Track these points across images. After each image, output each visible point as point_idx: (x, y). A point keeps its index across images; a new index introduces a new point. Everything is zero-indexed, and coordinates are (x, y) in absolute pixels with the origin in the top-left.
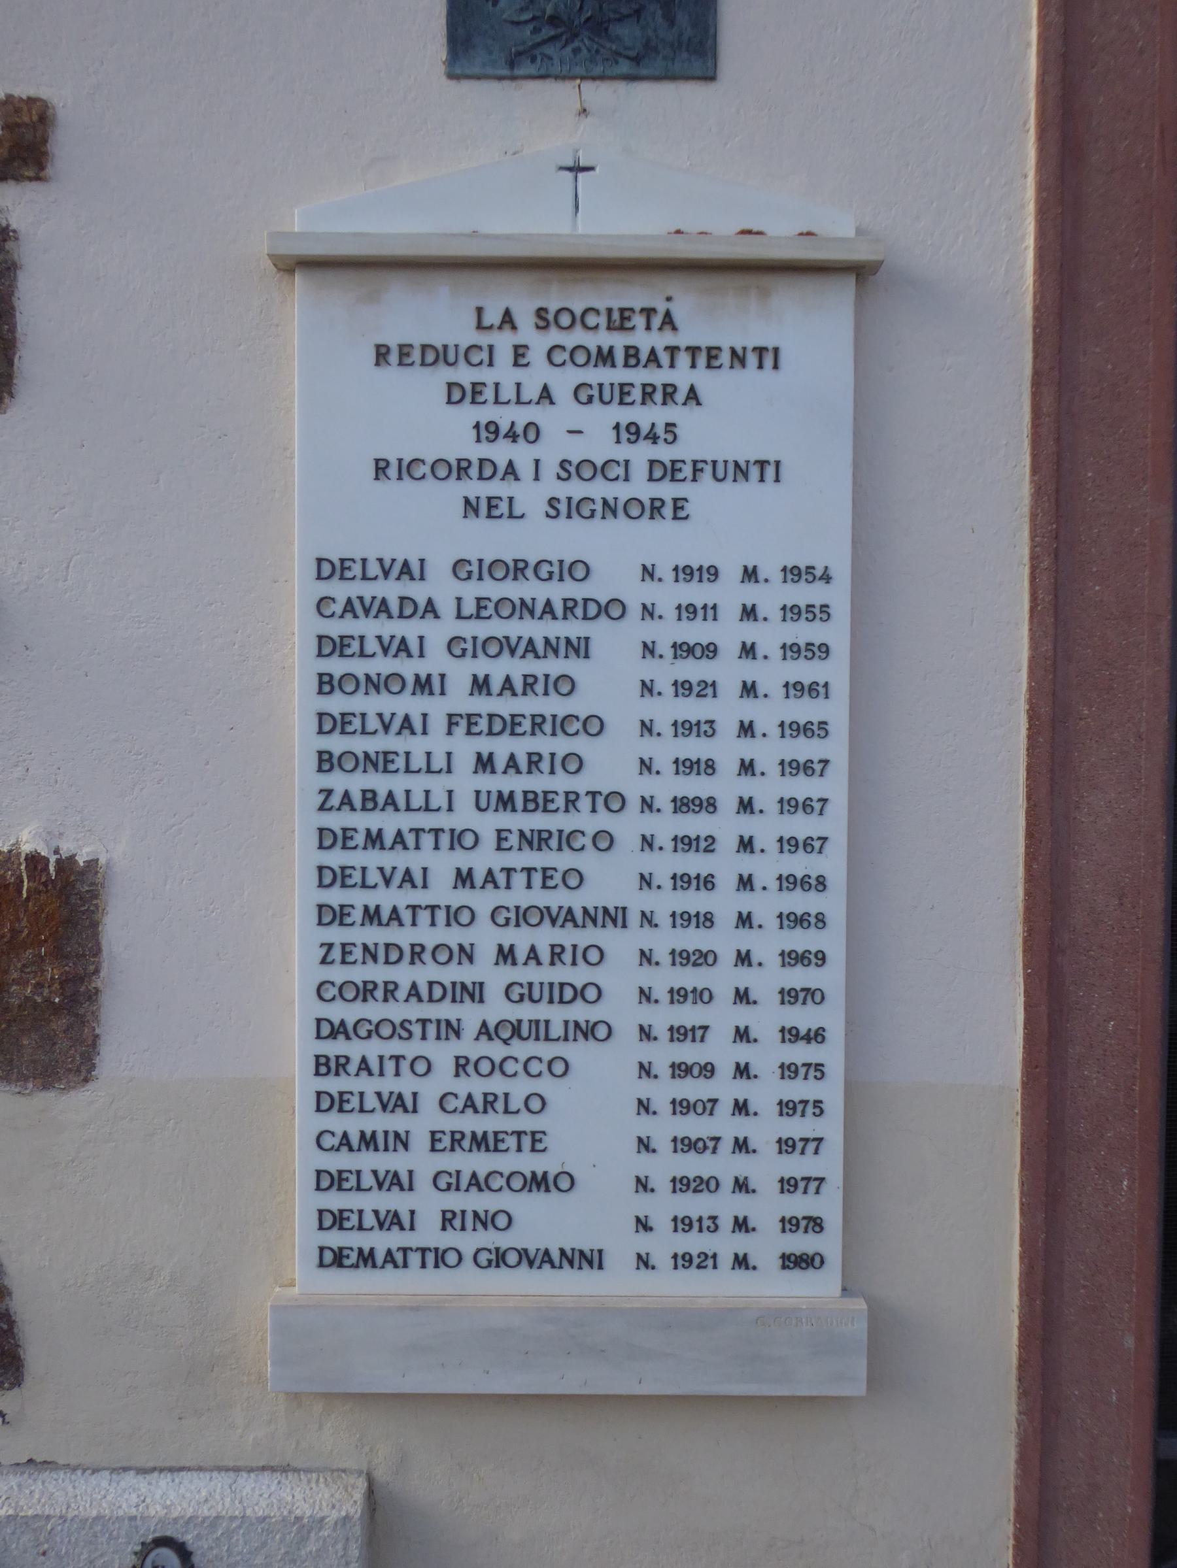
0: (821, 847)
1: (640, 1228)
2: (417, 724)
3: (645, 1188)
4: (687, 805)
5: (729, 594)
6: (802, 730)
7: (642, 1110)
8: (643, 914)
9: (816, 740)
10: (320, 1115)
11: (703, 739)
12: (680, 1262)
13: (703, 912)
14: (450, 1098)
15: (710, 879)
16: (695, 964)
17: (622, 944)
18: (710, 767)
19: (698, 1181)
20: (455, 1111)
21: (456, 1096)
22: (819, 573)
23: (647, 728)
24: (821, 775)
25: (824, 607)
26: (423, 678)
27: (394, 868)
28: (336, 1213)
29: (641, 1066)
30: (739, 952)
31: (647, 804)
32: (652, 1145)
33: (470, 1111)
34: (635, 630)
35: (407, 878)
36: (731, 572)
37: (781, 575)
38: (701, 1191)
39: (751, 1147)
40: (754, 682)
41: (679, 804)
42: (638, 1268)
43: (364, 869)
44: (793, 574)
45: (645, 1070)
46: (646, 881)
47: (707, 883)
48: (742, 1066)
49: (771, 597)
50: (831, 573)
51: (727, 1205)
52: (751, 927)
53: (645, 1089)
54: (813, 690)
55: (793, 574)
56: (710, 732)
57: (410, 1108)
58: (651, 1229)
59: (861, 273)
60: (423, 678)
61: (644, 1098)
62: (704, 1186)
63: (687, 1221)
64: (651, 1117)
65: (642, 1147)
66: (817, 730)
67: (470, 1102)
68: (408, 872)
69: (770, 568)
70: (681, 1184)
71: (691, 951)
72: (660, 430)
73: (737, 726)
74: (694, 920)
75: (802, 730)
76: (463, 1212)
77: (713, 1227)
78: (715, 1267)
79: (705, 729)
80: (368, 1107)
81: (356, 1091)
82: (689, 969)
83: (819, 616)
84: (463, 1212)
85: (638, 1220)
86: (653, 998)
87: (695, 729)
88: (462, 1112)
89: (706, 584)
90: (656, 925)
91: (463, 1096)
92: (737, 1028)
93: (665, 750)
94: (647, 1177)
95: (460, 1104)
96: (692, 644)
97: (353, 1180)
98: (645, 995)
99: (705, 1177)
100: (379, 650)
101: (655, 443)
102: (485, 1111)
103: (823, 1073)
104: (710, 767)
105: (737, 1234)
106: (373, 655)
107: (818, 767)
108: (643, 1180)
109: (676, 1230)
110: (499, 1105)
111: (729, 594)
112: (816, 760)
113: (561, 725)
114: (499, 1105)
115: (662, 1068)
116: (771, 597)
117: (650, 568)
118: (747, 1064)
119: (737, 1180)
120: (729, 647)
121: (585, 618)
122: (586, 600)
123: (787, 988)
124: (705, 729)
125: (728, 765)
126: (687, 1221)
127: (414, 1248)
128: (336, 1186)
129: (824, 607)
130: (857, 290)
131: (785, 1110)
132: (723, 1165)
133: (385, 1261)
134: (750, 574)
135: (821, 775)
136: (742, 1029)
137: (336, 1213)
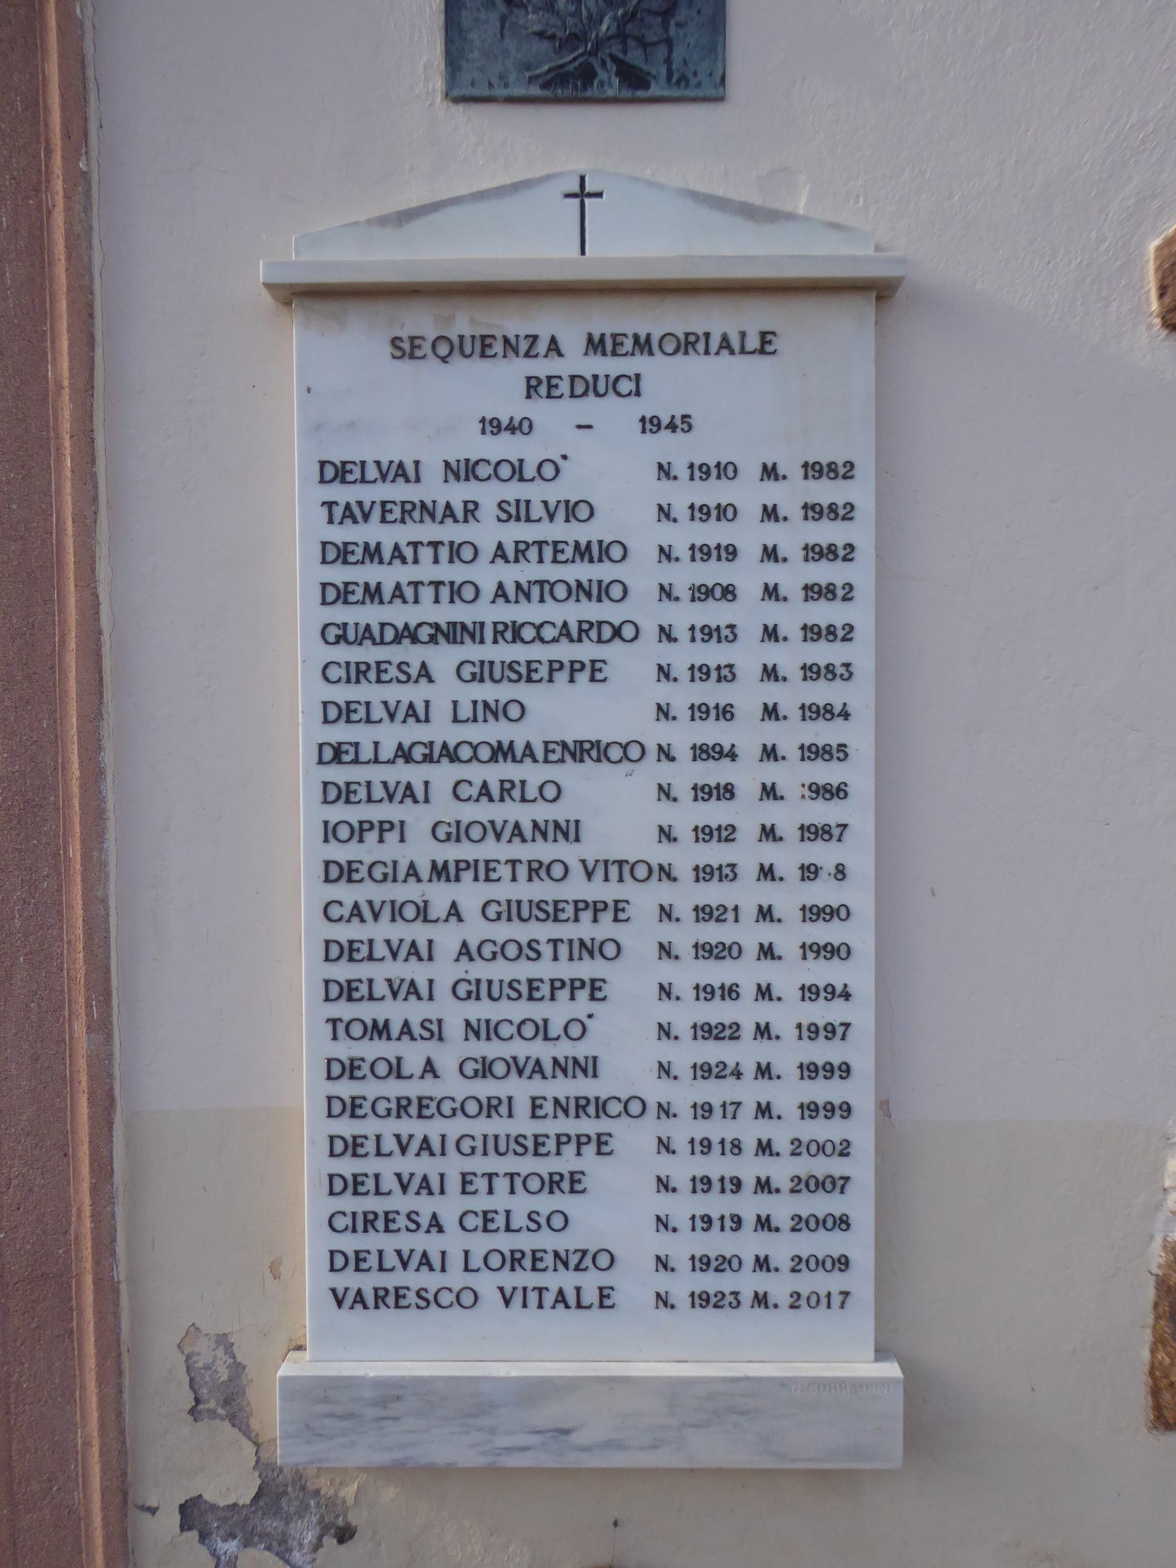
0: (841, 835)
1: (664, 638)
2: (435, 1185)
3: (667, 475)
4: (706, 752)
5: (748, 494)
6: (827, 553)
7: (664, 917)
8: (660, 748)
9: (835, 763)
10: (327, 726)
11: (724, 644)
12: (700, 1112)
13: (723, 783)
14: (464, 786)
15: (728, 708)
16: (718, 958)
17: (644, 899)
18: (731, 553)
19: (721, 947)
20: (469, 799)
21: (470, 783)
22: (837, 711)
23: (665, 553)
24: (839, 840)
25: (842, 747)
26: (440, 864)
27: (412, 1251)
28: (341, 546)
29: (659, 707)
30: (760, 1141)
31: (665, 753)
32: (673, 794)
33: (484, 799)
34: (651, 651)
35: (424, 1146)
36: (750, 469)
37: (801, 472)
38: (724, 958)
39: (776, 915)
40: (770, 906)
41: (698, 752)
42: (659, 680)
43: (380, 1252)
44: (813, 470)
45: (664, 672)
46: (663, 712)
47: (727, 792)
48: (763, 1067)
49: (789, 495)
50: (849, 709)
51: (751, 1092)
52: (771, 1117)
53: (666, 1011)
54: (831, 951)
55: (813, 470)
56: (731, 637)
57: (422, 717)
58: (675, 640)
59: (880, 291)
60: (440, 864)
61: (665, 625)
62: (726, 953)
63: (709, 989)
64: (671, 482)
65: (662, 1033)
66: (841, 513)
67: (485, 791)
68: (425, 1255)
69: (790, 466)
70: (704, 1071)
71: (714, 944)
72: (678, 421)
73: (758, 830)
74: (715, 792)
75: (827, 553)
76: (476, 861)
77: (735, 1303)
78: (736, 920)
79: (726, 634)
80: (374, 717)
81: (363, 781)
82: (711, 1043)
83: (836, 755)
84: (476, 861)
85: (661, 829)
86: (671, 715)
87: (715, 635)
88: (477, 800)
89: (724, 563)
90: (674, 1152)
91: (478, 783)
92: (763, 826)
93: (682, 696)
94: (669, 463)
95: (474, 791)
96: (710, 586)
97: (362, 711)
98: (664, 513)
99: (728, 1256)
100: (397, 1188)
101: (674, 431)
102: (502, 800)
103: (846, 755)
104: (731, 553)
105: (766, 683)
106: (392, 1270)
107: (836, 832)
108: (667, 550)
109: (698, 999)
110: (516, 793)
111: (748, 494)
112: (833, 825)
113: (581, 1106)
114: (516, 793)
115: (682, 790)
116: (789, 495)
117: (667, 588)
118: (769, 1140)
119: (757, 1258)
120: (750, 549)
121: (600, 641)
122: (600, 623)
123: (811, 462)
124: (726, 634)
125: (748, 829)
126: (709, 989)
127: (425, 541)
128: (341, 600)
129: (842, 747)
130: (877, 310)
131: (807, 835)
132: (746, 1053)
133: (393, 557)
134: (770, 472)
135: (839, 840)
136: (763, 1180)
137: (341, 546)
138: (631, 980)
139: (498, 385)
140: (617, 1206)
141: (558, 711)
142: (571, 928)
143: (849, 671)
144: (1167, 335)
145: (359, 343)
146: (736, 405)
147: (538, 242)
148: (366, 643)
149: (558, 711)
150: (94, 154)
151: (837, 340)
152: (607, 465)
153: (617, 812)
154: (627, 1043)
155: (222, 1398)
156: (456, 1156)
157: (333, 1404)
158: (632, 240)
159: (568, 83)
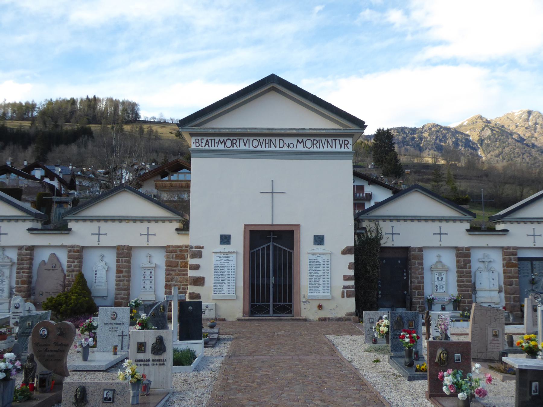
138: (321, 280)
139: (316, 256)
140: (320, 289)
141: (318, 269)
142: (318, 278)
143: (332, 147)
144: (426, 392)
145: (311, 255)
146: (325, 257)
147: (317, 251)
148: (311, 266)
149: (318, 269)
150: (462, 121)
151: (329, 255)
152: (320, 259)
153: (320, 273)
154: (321, 282)
155: (304, 297)
156: (314, 286)
157: (309, 296)
158: (320, 251)
159: (318, 245)
